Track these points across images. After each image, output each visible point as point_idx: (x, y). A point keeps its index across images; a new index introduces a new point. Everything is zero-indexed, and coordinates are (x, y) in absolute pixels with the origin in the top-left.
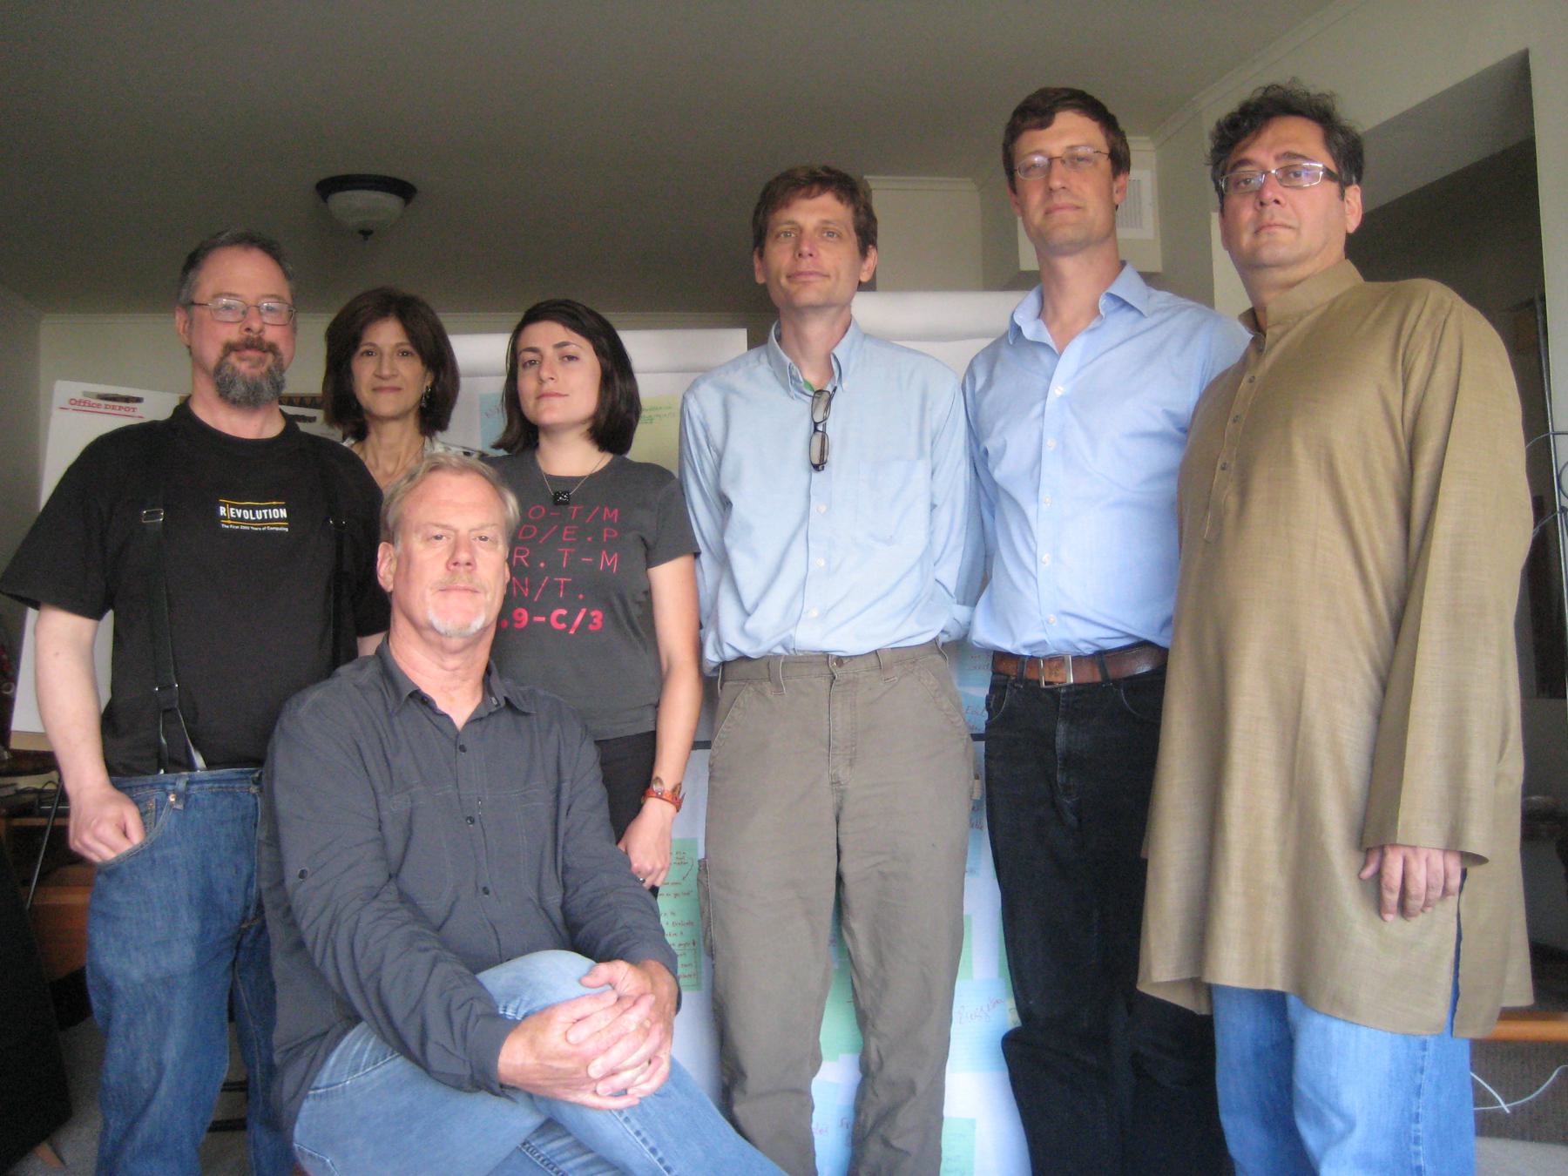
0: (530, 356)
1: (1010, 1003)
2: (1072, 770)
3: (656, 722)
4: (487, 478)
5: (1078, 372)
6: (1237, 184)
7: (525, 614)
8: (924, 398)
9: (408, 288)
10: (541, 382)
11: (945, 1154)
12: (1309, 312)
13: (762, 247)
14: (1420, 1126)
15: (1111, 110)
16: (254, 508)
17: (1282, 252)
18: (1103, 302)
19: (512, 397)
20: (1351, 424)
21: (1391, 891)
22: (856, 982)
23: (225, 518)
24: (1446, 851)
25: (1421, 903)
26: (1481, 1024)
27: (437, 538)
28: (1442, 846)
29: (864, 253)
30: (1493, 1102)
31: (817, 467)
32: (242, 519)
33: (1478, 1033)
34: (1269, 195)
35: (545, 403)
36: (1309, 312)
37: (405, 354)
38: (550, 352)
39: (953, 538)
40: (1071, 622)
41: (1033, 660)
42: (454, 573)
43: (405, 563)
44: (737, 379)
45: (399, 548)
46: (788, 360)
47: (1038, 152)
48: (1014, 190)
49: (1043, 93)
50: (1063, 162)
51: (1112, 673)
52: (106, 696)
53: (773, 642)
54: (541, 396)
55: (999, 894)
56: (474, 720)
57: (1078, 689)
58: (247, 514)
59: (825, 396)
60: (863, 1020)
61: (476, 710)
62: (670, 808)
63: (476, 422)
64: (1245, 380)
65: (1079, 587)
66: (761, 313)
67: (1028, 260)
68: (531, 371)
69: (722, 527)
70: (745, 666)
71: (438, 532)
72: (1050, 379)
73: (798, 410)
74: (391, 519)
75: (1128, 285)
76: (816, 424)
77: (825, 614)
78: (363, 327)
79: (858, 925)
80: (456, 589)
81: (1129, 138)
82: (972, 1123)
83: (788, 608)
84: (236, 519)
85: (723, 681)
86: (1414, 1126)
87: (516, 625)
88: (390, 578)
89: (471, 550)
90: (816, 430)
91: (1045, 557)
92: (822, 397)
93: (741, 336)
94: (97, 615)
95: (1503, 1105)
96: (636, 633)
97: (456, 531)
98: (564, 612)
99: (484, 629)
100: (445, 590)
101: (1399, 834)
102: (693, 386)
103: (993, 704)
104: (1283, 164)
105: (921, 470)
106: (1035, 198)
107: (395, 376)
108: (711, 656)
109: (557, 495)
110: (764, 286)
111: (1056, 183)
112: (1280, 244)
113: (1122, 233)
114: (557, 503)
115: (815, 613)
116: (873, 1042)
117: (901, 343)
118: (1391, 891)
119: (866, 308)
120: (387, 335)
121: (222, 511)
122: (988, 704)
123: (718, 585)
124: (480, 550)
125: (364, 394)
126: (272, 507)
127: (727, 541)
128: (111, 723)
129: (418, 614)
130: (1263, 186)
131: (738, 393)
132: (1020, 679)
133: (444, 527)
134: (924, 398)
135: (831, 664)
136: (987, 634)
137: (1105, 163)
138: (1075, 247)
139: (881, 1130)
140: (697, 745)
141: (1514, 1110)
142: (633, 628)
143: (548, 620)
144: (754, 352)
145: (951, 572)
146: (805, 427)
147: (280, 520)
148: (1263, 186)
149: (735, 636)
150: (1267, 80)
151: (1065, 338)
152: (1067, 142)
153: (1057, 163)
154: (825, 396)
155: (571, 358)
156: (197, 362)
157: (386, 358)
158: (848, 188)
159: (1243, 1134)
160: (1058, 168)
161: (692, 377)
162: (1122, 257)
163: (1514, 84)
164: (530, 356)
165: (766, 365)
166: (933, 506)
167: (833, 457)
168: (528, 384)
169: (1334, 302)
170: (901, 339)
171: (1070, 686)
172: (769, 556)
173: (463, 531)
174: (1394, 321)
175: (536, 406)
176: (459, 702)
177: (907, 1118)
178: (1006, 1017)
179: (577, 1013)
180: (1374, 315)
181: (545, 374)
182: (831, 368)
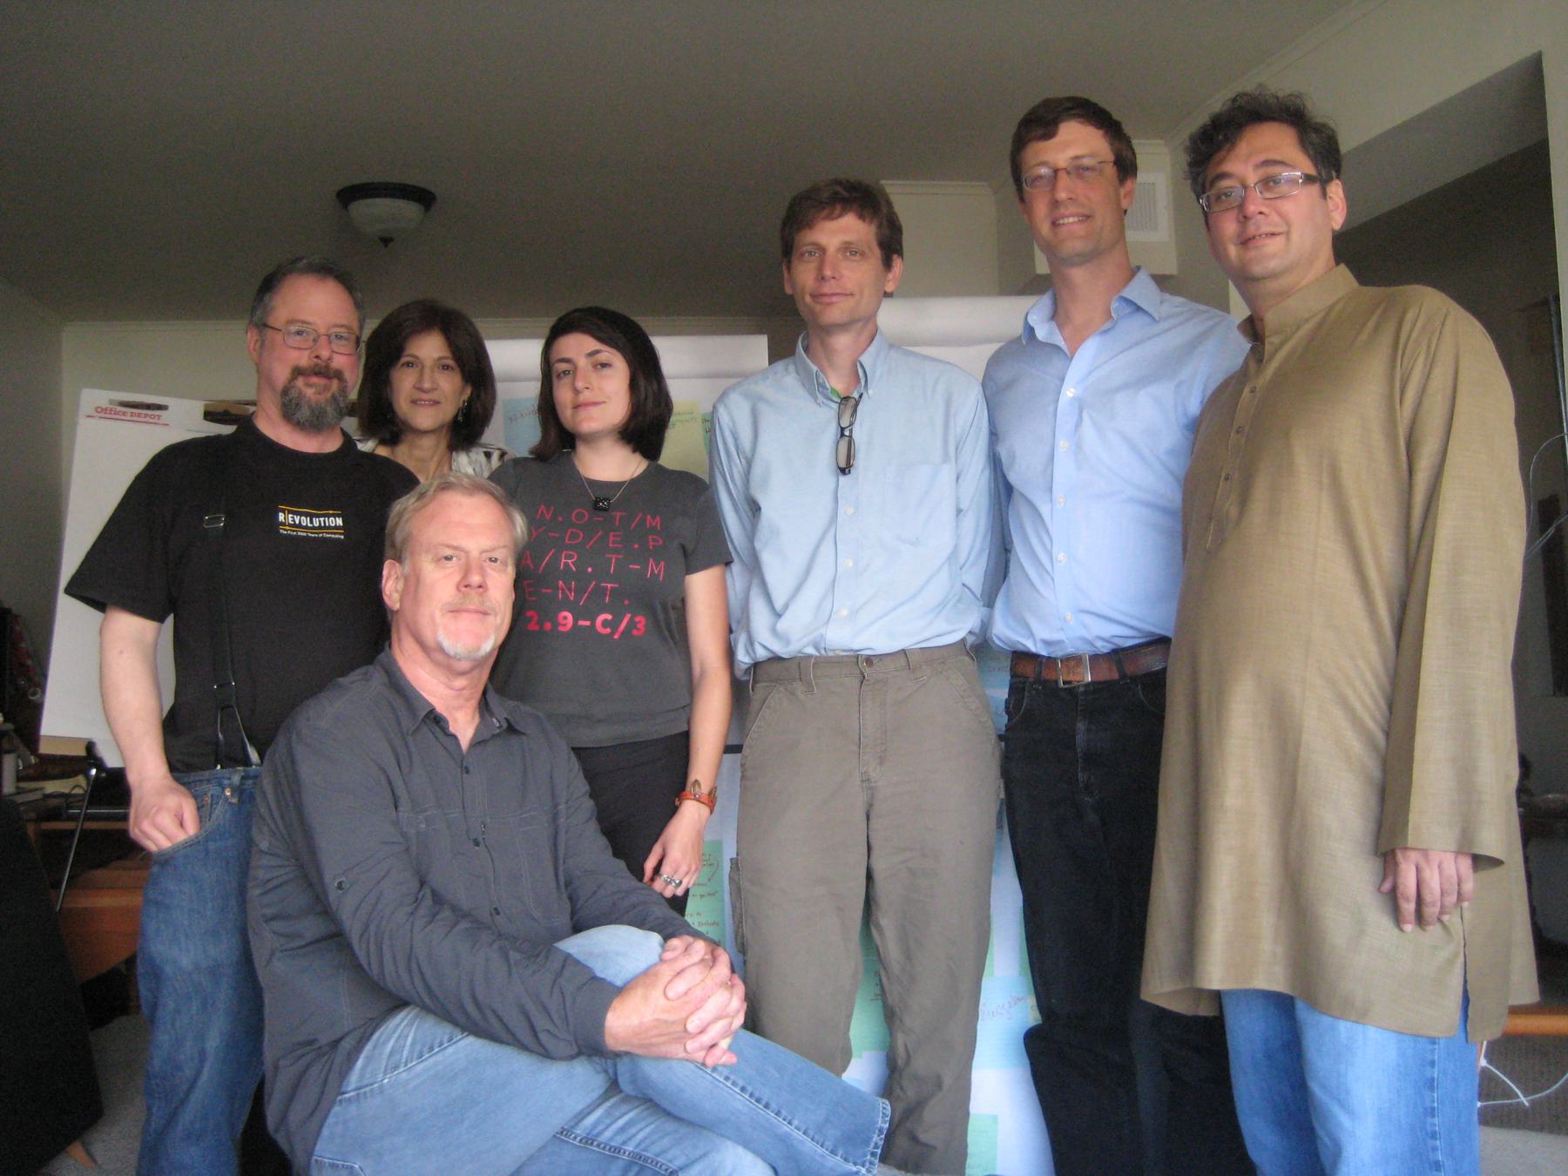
0: (563, 366)
1: (1031, 1001)
2: (1090, 766)
3: (689, 723)
4: (496, 498)
5: (1090, 373)
6: (1218, 198)
7: (570, 617)
8: (948, 404)
9: (451, 302)
10: (576, 392)
11: (970, 1150)
12: (1307, 320)
13: (789, 262)
14: (1436, 1120)
15: (1116, 116)
16: (312, 516)
17: (1273, 264)
18: (1115, 305)
19: (548, 407)
20: (1349, 434)
21: (1407, 900)
22: (884, 980)
24: (1459, 853)
25: (1437, 910)
26: (1493, 1027)
27: (448, 558)
28: (1453, 847)
29: (887, 264)
30: (1510, 1094)
31: (844, 471)
32: (300, 526)
33: (1495, 1032)
34: (1252, 208)
35: (583, 413)
36: (1307, 320)
37: (446, 367)
38: (582, 362)
39: (979, 541)
40: (1087, 619)
41: (1051, 661)
42: (465, 595)
43: (413, 584)
44: (764, 388)
45: (407, 567)
46: (815, 368)
47: (1044, 164)
48: (1022, 199)
49: (1047, 103)
50: (1068, 173)
51: (1130, 669)
52: (169, 701)
53: (805, 640)
54: (577, 407)
55: (1020, 897)
56: (477, 743)
57: (1096, 688)
58: (305, 521)
59: (852, 402)
60: (890, 1016)
61: (475, 735)
62: (705, 810)
63: (514, 431)
64: (1247, 390)
65: (1090, 589)
66: (788, 326)
67: (1042, 266)
68: (566, 380)
69: (751, 532)
70: (776, 667)
71: (448, 552)
72: (1063, 380)
73: (825, 416)
74: (399, 537)
75: (1142, 289)
76: (843, 429)
77: (854, 613)
78: (406, 338)
79: (886, 920)
80: (466, 611)
81: (1135, 142)
82: (995, 1119)
83: (819, 606)
84: (294, 525)
85: (755, 682)
86: (1429, 1120)
87: (561, 629)
88: (396, 596)
89: (483, 573)
90: (842, 435)
91: (1061, 556)
92: (849, 403)
93: (761, 343)
94: (161, 619)
95: (1522, 1099)
96: (672, 637)
97: (467, 553)
98: (609, 617)
99: (490, 653)
100: (456, 611)
101: (1410, 837)
102: (723, 396)
103: (1012, 707)
104: (1263, 172)
105: (947, 473)
106: (1041, 209)
107: (433, 390)
108: (743, 658)
109: (597, 502)
110: (791, 297)
111: (1062, 195)
112: (1272, 255)
113: (1131, 236)
114: (596, 507)
115: (845, 612)
116: (900, 1039)
117: (925, 346)
118: (1407, 900)
119: (891, 317)
120: (429, 348)
121: (281, 517)
122: (1007, 708)
123: (748, 589)
124: (489, 571)
125: (402, 405)
126: (329, 516)
127: (757, 545)
128: (172, 726)
129: (428, 635)
131: (766, 401)
132: (1038, 680)
133: (456, 548)
134: (948, 404)
135: (862, 665)
136: (1005, 632)
137: (1110, 171)
138: (1085, 258)
139: (908, 1125)
140: (730, 749)
141: (1533, 1102)
142: (670, 631)
143: (593, 624)
144: (780, 365)
145: (975, 577)
146: (831, 432)
147: (336, 527)
149: (767, 637)
150: (1240, 89)
151: (1076, 343)
152: (1071, 152)
153: (1062, 175)
154: (852, 402)
155: (604, 365)
156: (264, 376)
157: (427, 371)
158: (863, 198)
159: (1260, 1135)
160: (1064, 181)
161: (725, 383)
162: (1134, 263)
163: (1528, 86)
164: (563, 366)
165: (794, 374)
166: (959, 511)
167: (860, 462)
168: (563, 395)
169: (1330, 309)
170: (916, 344)
171: (1088, 684)
172: (800, 561)
173: (475, 553)
174: (1390, 328)
175: (573, 415)
176: (464, 726)
177: (933, 1113)
178: (1027, 1014)
180: (1371, 324)
181: (580, 385)
182: (858, 376)
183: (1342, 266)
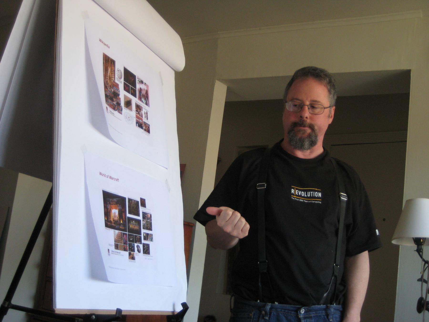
23: (293, 194)
84: (298, 196)
130: (113, 101)
148: (113, 101)
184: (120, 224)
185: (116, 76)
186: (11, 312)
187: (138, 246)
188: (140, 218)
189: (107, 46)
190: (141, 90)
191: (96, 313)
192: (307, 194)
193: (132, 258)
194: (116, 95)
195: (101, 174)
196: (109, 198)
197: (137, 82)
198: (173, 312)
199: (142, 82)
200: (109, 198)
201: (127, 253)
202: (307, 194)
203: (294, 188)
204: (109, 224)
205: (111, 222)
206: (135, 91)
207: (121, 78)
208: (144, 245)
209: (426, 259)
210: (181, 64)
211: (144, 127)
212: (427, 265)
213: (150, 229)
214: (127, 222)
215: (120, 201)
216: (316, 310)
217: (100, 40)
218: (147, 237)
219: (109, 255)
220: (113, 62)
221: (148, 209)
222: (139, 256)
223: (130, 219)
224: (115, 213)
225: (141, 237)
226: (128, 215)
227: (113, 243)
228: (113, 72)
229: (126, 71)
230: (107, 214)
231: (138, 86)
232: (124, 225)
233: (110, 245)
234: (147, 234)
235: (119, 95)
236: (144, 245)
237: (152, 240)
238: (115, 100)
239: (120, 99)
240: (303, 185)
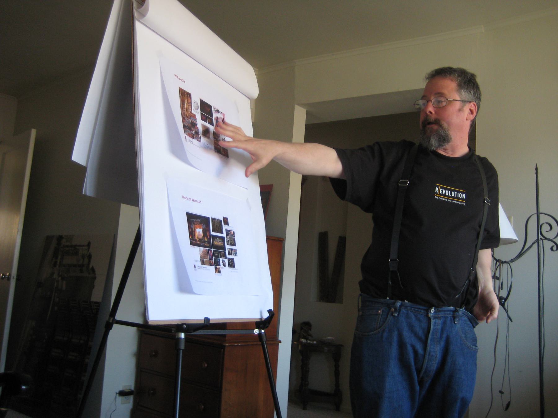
16: (451, 191)
23: (437, 193)
32: (445, 195)
58: (448, 193)
84: (442, 195)
126: (459, 192)
130: (191, 130)
147: (462, 199)
148: (191, 130)
179: (198, 113)
183: (280, 339)
184: (205, 242)
185: (193, 108)
186: (115, 326)
187: (223, 261)
188: (224, 235)
189: (182, 80)
190: (217, 119)
191: (187, 323)
192: (451, 194)
193: (219, 272)
194: (194, 125)
195: (183, 197)
196: (192, 218)
197: (213, 111)
198: (261, 319)
199: (218, 111)
200: (192, 218)
201: (213, 268)
202: (451, 194)
203: (438, 187)
204: (194, 242)
205: (195, 240)
206: (212, 120)
207: (198, 109)
208: (229, 259)
209: (497, 258)
210: (254, 91)
211: (223, 152)
212: (498, 263)
213: (234, 245)
214: (211, 239)
215: (204, 221)
216: (445, 311)
217: (175, 76)
218: (231, 252)
219: (195, 270)
220: (189, 95)
221: (231, 227)
222: (225, 270)
223: (214, 237)
224: (199, 232)
225: (225, 253)
226: (212, 233)
227: (199, 259)
228: (190, 104)
229: (202, 102)
230: (192, 233)
231: (215, 115)
232: (209, 242)
233: (196, 261)
234: (232, 250)
235: (196, 125)
236: (229, 259)
237: (236, 254)
238: (193, 129)
239: (198, 128)
240: (449, 182)
